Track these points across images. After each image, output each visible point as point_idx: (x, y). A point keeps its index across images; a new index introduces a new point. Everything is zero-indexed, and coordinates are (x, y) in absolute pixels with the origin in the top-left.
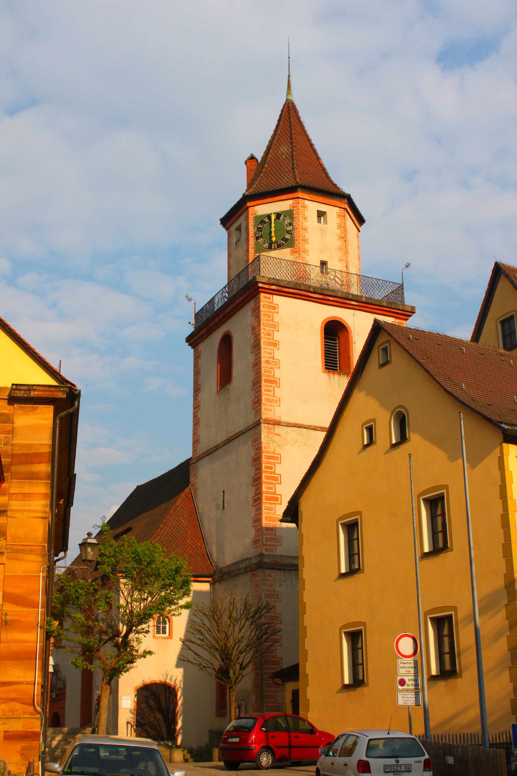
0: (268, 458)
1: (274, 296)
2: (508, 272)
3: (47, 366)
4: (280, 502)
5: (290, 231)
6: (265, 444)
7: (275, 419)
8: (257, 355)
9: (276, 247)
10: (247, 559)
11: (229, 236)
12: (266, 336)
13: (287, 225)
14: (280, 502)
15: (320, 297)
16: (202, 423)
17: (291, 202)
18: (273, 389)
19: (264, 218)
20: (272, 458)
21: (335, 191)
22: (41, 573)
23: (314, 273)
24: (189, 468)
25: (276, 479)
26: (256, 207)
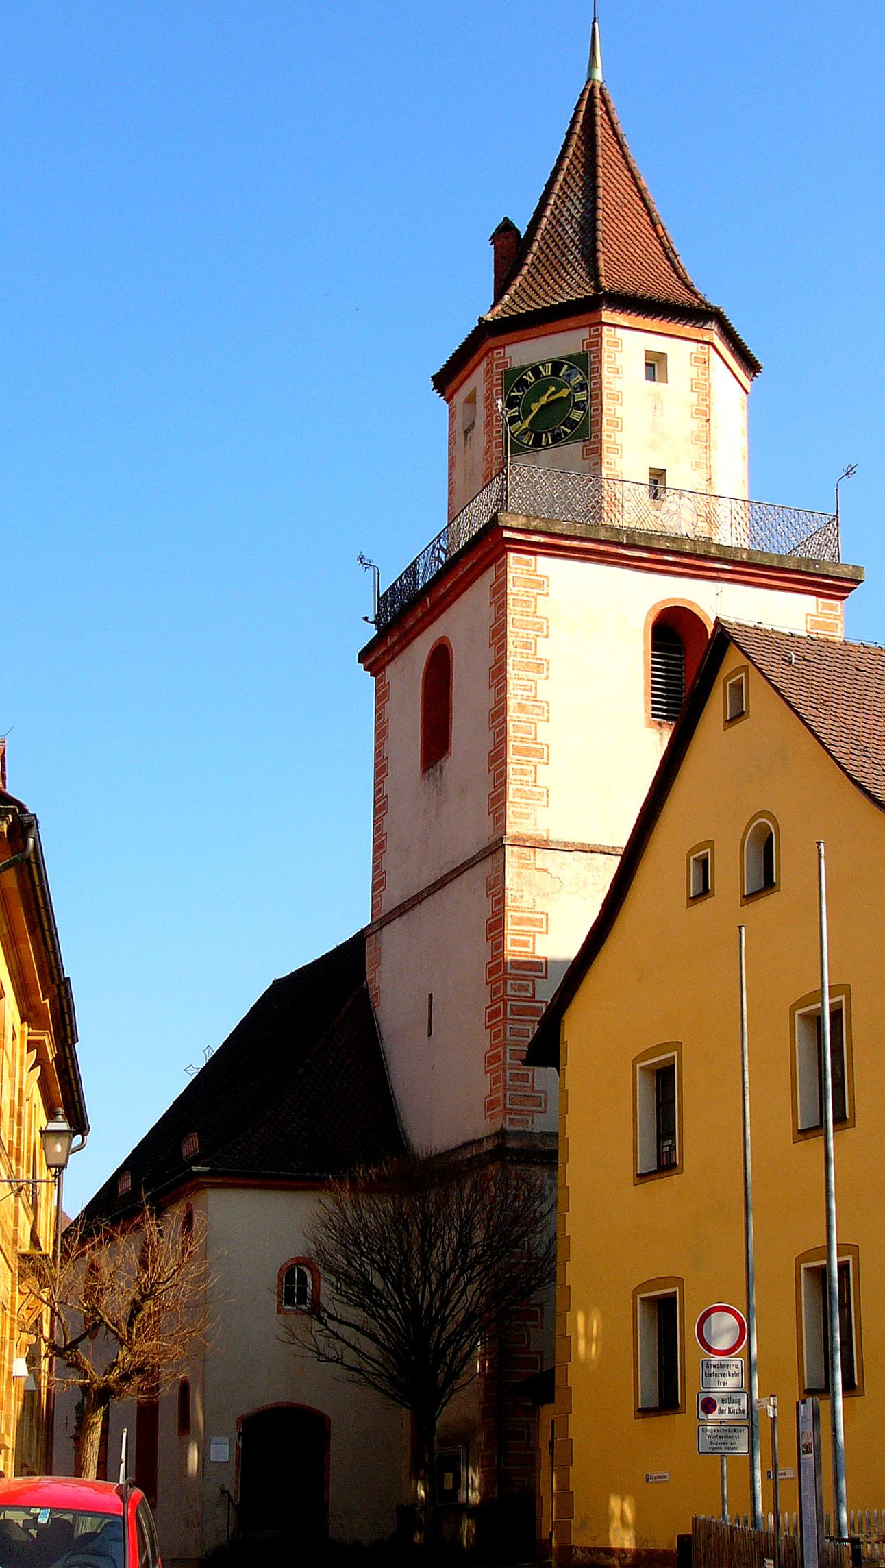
0: (520, 921)
1: (540, 558)
6: (513, 892)
7: (537, 835)
8: (499, 692)
12: (518, 650)
13: (575, 389)
15: (645, 555)
16: (390, 845)
18: (533, 769)
19: (526, 374)
23: (632, 500)
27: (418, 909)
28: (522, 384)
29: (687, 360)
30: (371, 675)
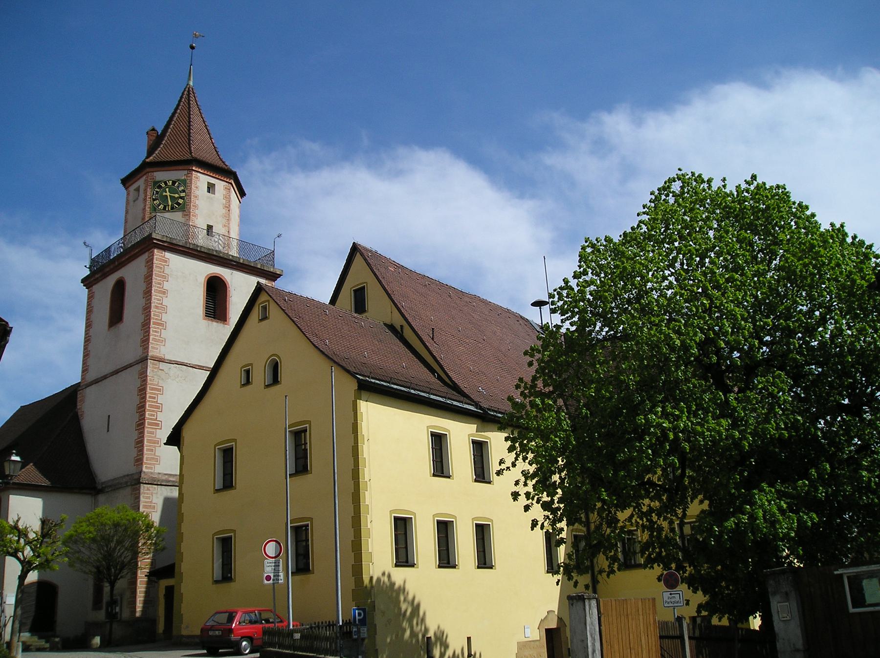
0: (152, 389)
2: (363, 251)
4: (160, 428)
5: (183, 197)
10: (128, 475)
11: (128, 194)
14: (160, 428)
21: (222, 165)
24: (77, 394)
26: (155, 173)
28: (160, 187)
29: (222, 188)
30: (84, 286)
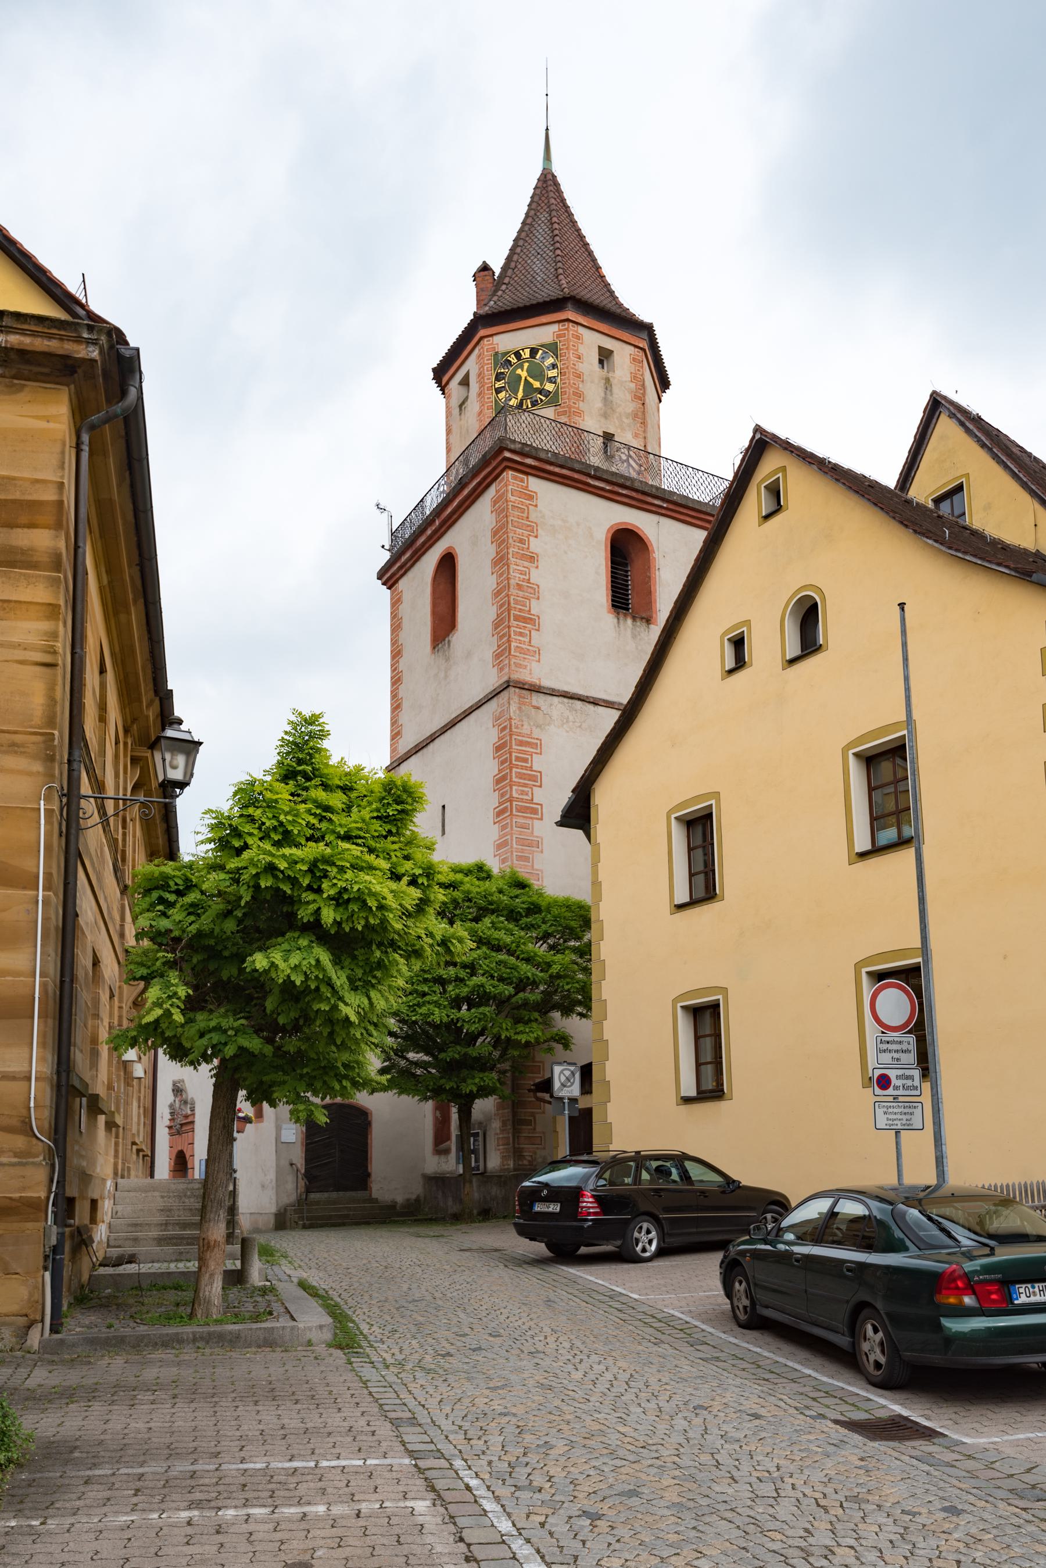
0: (521, 743)
3: (44, 279)
9: (530, 406)
16: (405, 705)
17: (555, 327)
20: (528, 744)
22: (42, 802)
25: (533, 778)
27: (431, 745)
